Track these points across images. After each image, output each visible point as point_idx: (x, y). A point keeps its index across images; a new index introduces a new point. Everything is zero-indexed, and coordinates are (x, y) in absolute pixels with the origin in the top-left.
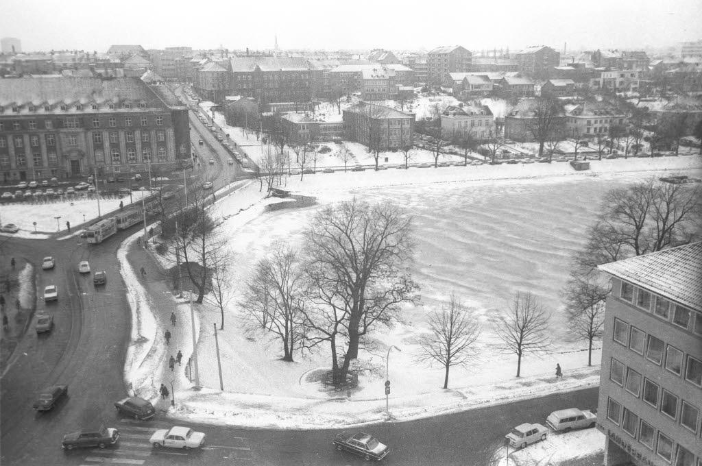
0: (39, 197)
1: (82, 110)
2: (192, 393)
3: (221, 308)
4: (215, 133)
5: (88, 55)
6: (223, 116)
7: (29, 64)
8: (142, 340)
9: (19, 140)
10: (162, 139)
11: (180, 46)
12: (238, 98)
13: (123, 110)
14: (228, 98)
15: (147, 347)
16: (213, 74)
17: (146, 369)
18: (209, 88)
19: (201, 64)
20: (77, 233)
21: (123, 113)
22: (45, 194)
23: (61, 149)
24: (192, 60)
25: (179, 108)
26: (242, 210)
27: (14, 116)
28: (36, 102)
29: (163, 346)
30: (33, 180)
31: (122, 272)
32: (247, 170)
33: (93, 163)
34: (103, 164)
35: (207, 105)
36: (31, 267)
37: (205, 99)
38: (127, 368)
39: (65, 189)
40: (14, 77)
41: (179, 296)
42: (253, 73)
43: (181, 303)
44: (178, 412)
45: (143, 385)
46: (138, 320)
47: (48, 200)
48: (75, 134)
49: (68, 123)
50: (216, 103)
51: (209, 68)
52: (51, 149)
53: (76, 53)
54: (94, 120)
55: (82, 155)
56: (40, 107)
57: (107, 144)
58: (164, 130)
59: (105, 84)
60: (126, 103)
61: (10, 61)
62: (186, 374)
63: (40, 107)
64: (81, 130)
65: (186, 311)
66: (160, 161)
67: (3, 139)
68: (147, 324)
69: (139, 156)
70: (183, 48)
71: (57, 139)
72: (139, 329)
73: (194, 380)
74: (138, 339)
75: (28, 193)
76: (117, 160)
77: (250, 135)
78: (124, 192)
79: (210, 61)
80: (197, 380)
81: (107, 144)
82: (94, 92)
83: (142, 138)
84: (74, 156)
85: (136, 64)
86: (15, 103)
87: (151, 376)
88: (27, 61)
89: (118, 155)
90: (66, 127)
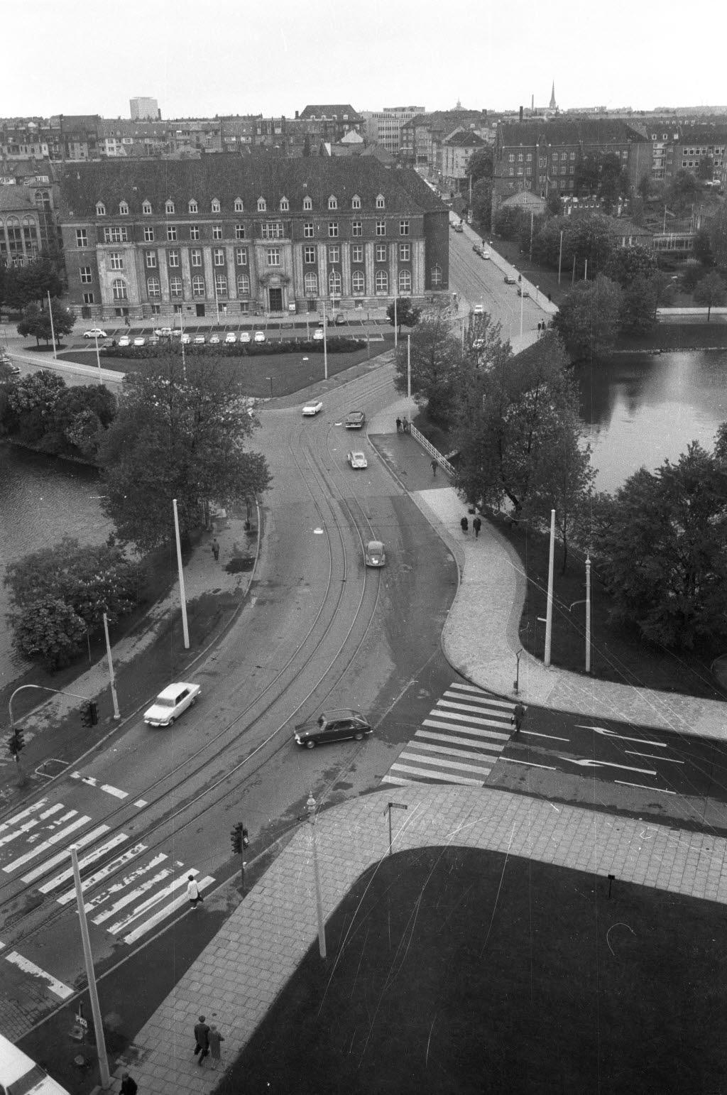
23: (256, 269)
48: (278, 248)
49: (268, 229)
52: (242, 271)
54: (307, 226)
55: (286, 280)
58: (411, 244)
64: (288, 241)
83: (376, 255)
84: (275, 281)
90: (265, 237)
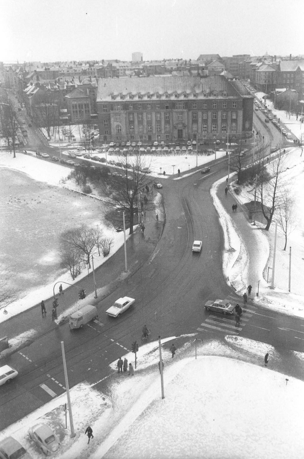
0: (160, 151)
1: (142, 98)
2: (269, 290)
3: (286, 236)
4: (266, 114)
5: (186, 61)
6: (272, 103)
7: (151, 68)
8: (232, 250)
9: (149, 116)
10: (234, 117)
11: (242, 54)
12: (284, 90)
13: (212, 98)
14: (277, 90)
15: (236, 255)
16: (266, 74)
17: (237, 268)
18: (262, 82)
19: (257, 66)
20: (185, 176)
21: (212, 100)
22: (163, 150)
24: (251, 64)
25: (247, 96)
26: (288, 168)
27: (149, 101)
28: (161, 92)
29: (246, 256)
30: (156, 141)
31: (214, 204)
32: (290, 141)
33: (190, 131)
34: (196, 132)
35: (260, 95)
36: (160, 195)
37: (259, 90)
38: (224, 266)
39: (175, 148)
40: (144, 77)
41: (253, 223)
42: (295, 72)
43: (255, 229)
44: (261, 301)
45: (236, 280)
46: (229, 237)
47: (165, 154)
48: (182, 113)
50: (267, 93)
51: (263, 69)
52: (167, 122)
53: (179, 60)
55: (184, 126)
56: (163, 95)
57: (200, 120)
59: (203, 80)
60: (215, 93)
61: (141, 67)
62: (264, 277)
63: (163, 95)
65: (259, 234)
66: (232, 132)
67: (141, 115)
68: (233, 239)
69: (219, 129)
70: (244, 55)
71: (171, 115)
72: (229, 243)
73: (269, 282)
74: (229, 249)
75: (154, 149)
76: (205, 130)
77: (291, 117)
78: (210, 152)
79: (264, 64)
80: (272, 281)
81: (200, 120)
82: (195, 85)
83: (222, 116)
84: (180, 126)
85: (216, 67)
86: (149, 93)
87: (240, 274)
88: (150, 66)
89: (206, 127)
90: (177, 108)
